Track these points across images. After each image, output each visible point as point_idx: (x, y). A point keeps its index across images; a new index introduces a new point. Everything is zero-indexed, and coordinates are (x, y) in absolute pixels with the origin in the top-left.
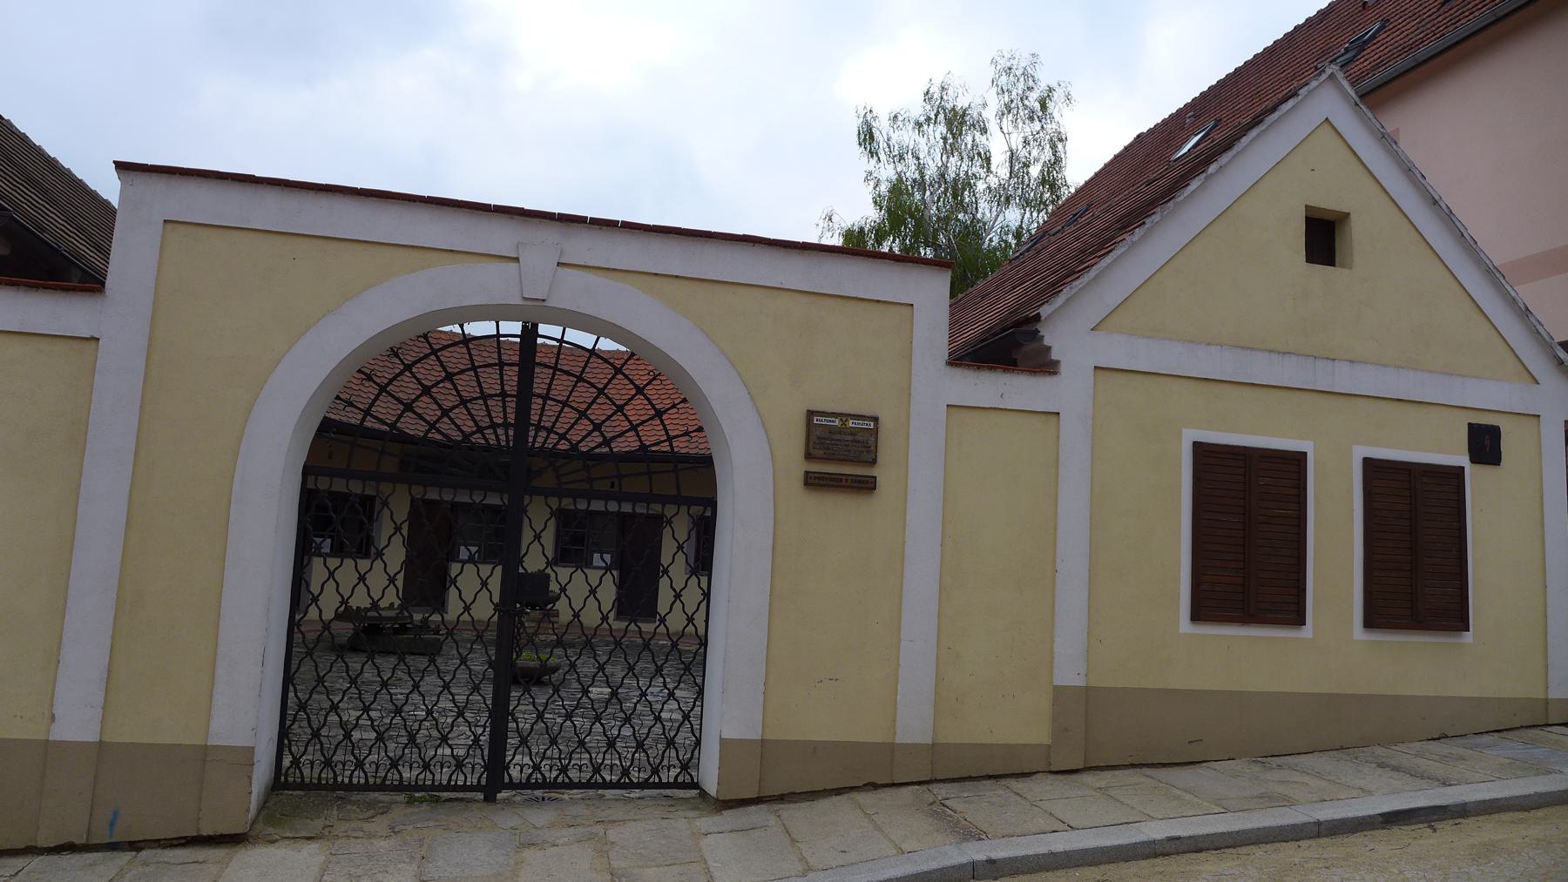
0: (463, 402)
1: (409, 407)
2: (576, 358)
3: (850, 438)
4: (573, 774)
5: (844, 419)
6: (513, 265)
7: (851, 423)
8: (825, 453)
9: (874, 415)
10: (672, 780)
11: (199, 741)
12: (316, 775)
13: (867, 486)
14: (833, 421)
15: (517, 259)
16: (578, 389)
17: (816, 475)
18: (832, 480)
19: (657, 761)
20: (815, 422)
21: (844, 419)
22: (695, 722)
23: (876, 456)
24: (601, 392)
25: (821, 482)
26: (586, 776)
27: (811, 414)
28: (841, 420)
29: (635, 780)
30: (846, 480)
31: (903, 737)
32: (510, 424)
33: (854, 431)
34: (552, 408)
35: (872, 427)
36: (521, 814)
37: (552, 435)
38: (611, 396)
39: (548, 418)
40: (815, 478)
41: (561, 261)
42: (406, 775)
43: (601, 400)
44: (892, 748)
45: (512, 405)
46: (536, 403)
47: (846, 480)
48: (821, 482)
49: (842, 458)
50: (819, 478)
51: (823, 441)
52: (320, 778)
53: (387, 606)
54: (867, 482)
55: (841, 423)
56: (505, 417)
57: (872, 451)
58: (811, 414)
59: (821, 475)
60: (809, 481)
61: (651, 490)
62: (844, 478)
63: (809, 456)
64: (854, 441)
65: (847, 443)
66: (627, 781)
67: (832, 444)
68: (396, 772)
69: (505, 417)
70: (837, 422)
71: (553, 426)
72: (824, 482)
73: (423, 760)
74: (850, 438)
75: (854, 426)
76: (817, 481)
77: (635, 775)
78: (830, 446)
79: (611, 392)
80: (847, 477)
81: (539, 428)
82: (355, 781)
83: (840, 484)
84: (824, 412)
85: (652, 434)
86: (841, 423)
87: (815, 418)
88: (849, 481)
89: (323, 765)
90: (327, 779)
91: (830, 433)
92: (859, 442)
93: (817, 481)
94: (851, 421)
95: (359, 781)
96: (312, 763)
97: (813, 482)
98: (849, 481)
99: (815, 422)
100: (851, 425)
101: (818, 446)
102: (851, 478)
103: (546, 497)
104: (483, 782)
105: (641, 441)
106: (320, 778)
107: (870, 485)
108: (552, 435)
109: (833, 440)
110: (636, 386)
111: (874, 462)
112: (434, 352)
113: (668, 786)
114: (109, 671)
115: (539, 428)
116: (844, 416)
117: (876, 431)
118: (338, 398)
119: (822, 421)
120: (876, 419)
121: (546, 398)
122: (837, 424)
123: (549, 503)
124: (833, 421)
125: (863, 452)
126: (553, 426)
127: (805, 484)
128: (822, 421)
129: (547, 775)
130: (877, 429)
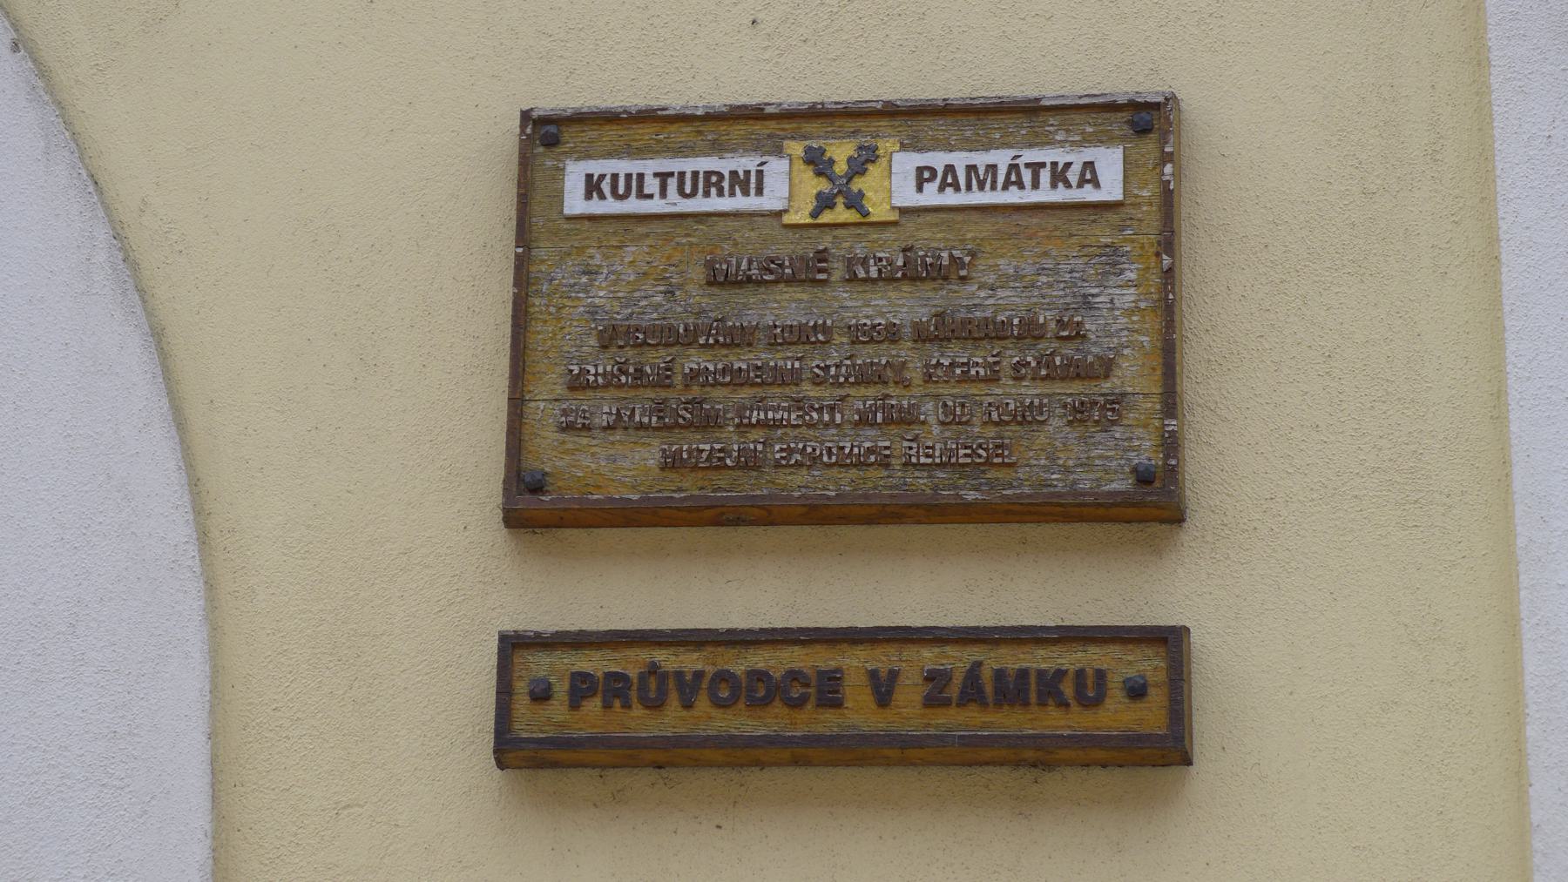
5: (841, 153)
8: (672, 463)
9: (1148, 87)
14: (740, 182)
17: (595, 663)
20: (575, 202)
21: (841, 153)
23: (1171, 445)
25: (638, 722)
28: (817, 162)
30: (883, 688)
35: (1111, 188)
40: (582, 687)
47: (883, 688)
48: (638, 722)
49: (831, 485)
50: (615, 688)
51: (655, 359)
53: (853, 210)
54: (1091, 690)
55: (813, 185)
57: (1116, 403)
59: (631, 663)
60: (529, 721)
62: (855, 662)
65: (881, 355)
67: (738, 379)
72: (672, 721)
75: (931, 196)
76: (593, 717)
78: (721, 398)
80: (881, 659)
83: (828, 722)
84: (647, 116)
86: (813, 185)
87: (575, 174)
88: (909, 694)
91: (720, 279)
92: (993, 332)
93: (593, 717)
98: (909, 694)
99: (575, 202)
100: (906, 195)
101: (604, 409)
102: (928, 656)
109: (740, 338)
119: (636, 185)
122: (773, 198)
124: (740, 182)
125: (1027, 417)
127: (514, 520)
128: (636, 185)
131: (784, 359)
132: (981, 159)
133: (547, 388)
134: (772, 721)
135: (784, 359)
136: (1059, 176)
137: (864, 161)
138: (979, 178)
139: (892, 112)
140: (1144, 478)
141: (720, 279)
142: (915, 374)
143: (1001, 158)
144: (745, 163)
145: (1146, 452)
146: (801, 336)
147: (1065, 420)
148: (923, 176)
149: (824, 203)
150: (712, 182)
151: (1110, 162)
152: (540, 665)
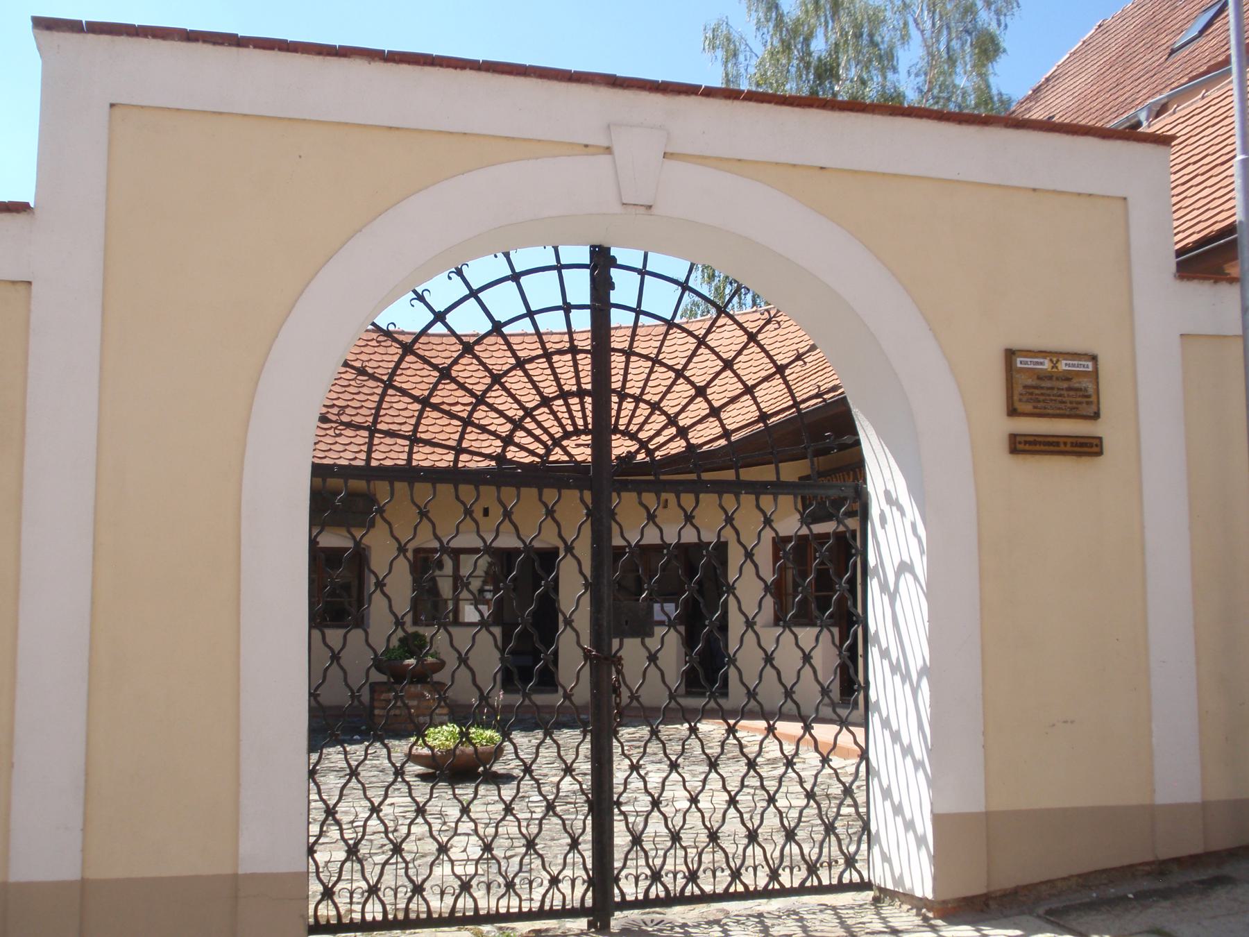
0: (520, 364)
1: (445, 374)
2: (434, 347)
3: (1065, 385)
4: (785, 879)
6: (604, 159)
7: (1063, 366)
10: (835, 881)
11: (228, 870)
12: (402, 905)
13: (1089, 448)
15: (608, 150)
16: (439, 393)
18: (1030, 443)
19: (739, 862)
21: (1055, 360)
22: (861, 798)
24: (701, 342)
26: (762, 881)
27: (1010, 354)
28: (1051, 361)
29: (788, 885)
31: (1164, 797)
32: (587, 393)
33: (1067, 377)
34: (639, 368)
35: (1090, 369)
36: (1061, 923)
37: (642, 405)
38: (514, 392)
39: (636, 378)
41: (669, 150)
42: (482, 904)
43: (702, 350)
44: (1152, 811)
45: (585, 362)
46: (617, 361)
47: (1065, 444)
52: (407, 910)
56: (578, 383)
58: (1010, 354)
61: (778, 477)
63: (1012, 412)
64: (1069, 389)
65: (1062, 392)
66: (777, 886)
68: (421, 901)
69: (578, 383)
70: (1047, 365)
71: (642, 393)
73: (505, 878)
74: (1065, 385)
75: (1067, 368)
77: (785, 879)
79: (478, 389)
80: (1065, 440)
81: (623, 396)
82: (652, 895)
85: (773, 397)
87: (1019, 360)
89: (366, 894)
90: (418, 912)
94: (1064, 362)
95: (520, 907)
96: (573, 881)
97: (1020, 445)
99: (1019, 365)
101: (1024, 398)
103: (639, 494)
104: (589, 902)
105: (759, 409)
106: (407, 910)
107: (1095, 449)
108: (642, 405)
110: (416, 399)
111: (1096, 416)
112: (474, 294)
113: (830, 889)
114: (87, 774)
115: (623, 396)
116: (1055, 355)
117: (1095, 374)
118: (346, 364)
120: (1094, 358)
121: (629, 353)
122: (1046, 366)
123: (644, 502)
126: (642, 393)
129: (671, 887)
130: (1096, 371)
131: (1048, 392)
132: (1074, 362)
133: (354, 592)
134: (1052, 448)
135: (1048, 392)
136: (1084, 366)
137: (1058, 361)
138: (1073, 365)
139: (1061, 353)
140: (1095, 413)
141: (1039, 378)
142: (1069, 445)
143: (1076, 362)
144: (1042, 360)
145: (1096, 410)
146: (1052, 388)
147: (753, 13)
148: (1066, 364)
149: (1053, 368)
150: (1037, 363)
151: (1090, 364)
152: (1018, 439)
